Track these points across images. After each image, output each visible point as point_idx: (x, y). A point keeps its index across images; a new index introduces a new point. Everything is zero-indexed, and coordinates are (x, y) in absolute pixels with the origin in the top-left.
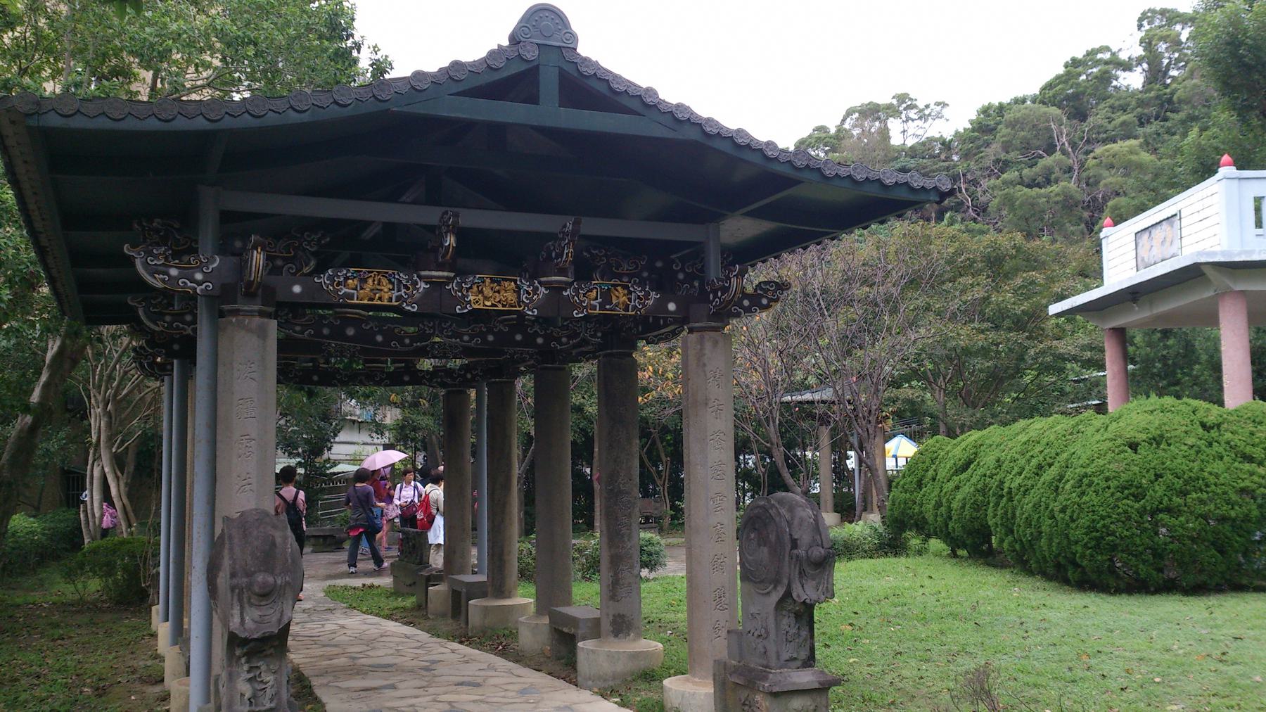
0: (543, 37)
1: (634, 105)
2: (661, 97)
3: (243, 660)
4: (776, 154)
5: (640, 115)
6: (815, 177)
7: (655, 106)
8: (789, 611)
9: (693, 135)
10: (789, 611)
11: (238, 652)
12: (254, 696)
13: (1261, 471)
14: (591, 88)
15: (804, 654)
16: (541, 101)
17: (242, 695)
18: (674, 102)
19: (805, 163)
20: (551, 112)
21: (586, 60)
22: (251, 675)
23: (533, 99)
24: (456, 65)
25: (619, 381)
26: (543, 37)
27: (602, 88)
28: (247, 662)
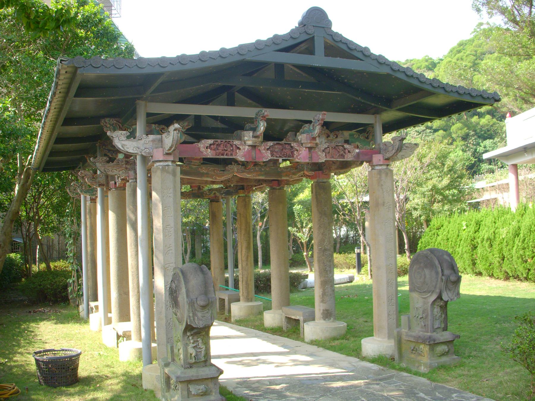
0: (316, 18)
1: (359, 55)
2: (372, 52)
3: (190, 338)
4: (425, 80)
5: (361, 60)
6: (441, 91)
7: (369, 56)
8: (438, 305)
9: (384, 70)
10: (438, 305)
11: (188, 334)
12: (197, 355)
13: (2, 361)
14: (341, 48)
15: (443, 326)
16: (316, 53)
17: (191, 354)
18: (378, 54)
19: (438, 85)
20: (319, 60)
21: (337, 34)
22: (195, 345)
23: (311, 51)
24: (276, 37)
25: (322, 190)
26: (316, 18)
27: (344, 47)
28: (192, 339)
